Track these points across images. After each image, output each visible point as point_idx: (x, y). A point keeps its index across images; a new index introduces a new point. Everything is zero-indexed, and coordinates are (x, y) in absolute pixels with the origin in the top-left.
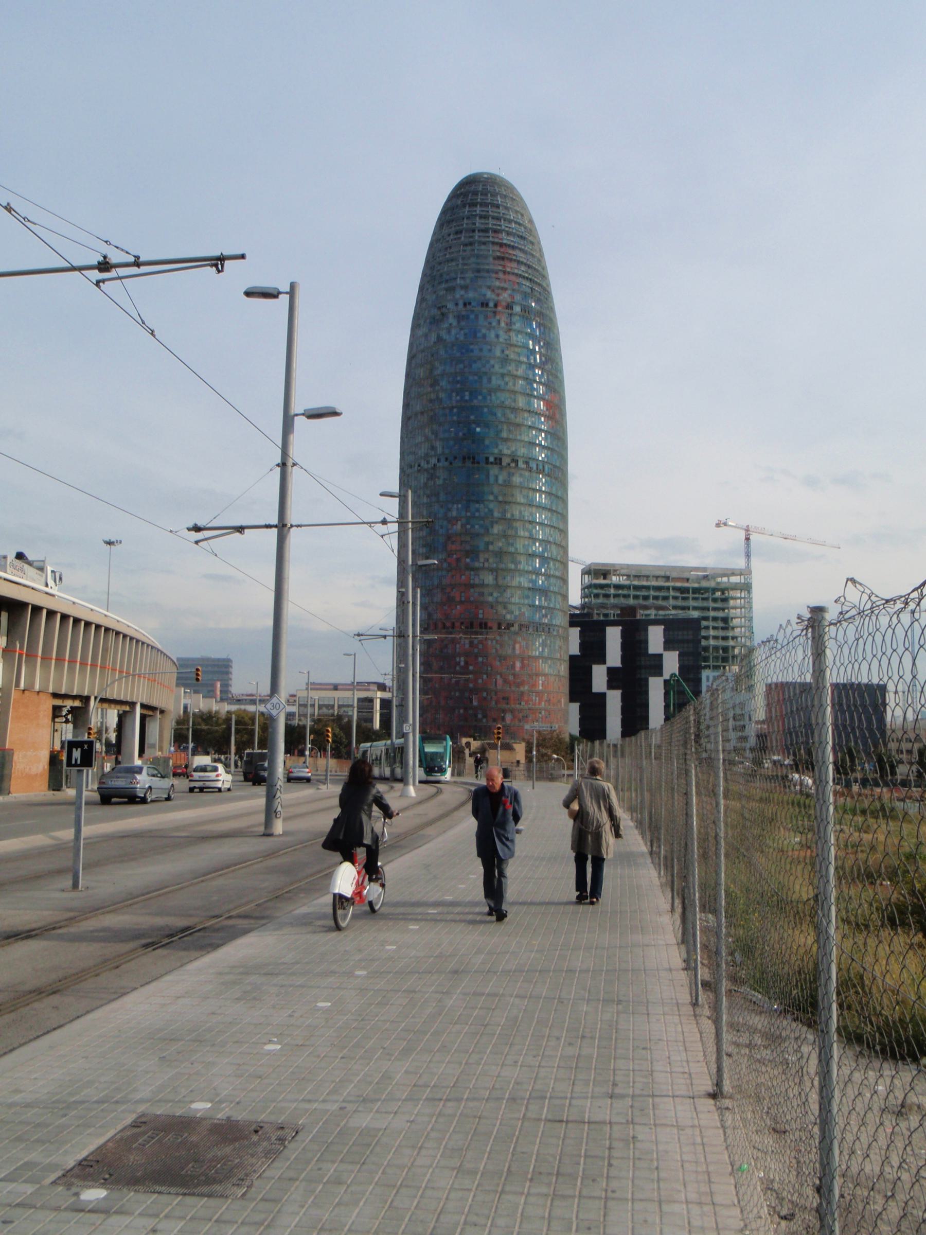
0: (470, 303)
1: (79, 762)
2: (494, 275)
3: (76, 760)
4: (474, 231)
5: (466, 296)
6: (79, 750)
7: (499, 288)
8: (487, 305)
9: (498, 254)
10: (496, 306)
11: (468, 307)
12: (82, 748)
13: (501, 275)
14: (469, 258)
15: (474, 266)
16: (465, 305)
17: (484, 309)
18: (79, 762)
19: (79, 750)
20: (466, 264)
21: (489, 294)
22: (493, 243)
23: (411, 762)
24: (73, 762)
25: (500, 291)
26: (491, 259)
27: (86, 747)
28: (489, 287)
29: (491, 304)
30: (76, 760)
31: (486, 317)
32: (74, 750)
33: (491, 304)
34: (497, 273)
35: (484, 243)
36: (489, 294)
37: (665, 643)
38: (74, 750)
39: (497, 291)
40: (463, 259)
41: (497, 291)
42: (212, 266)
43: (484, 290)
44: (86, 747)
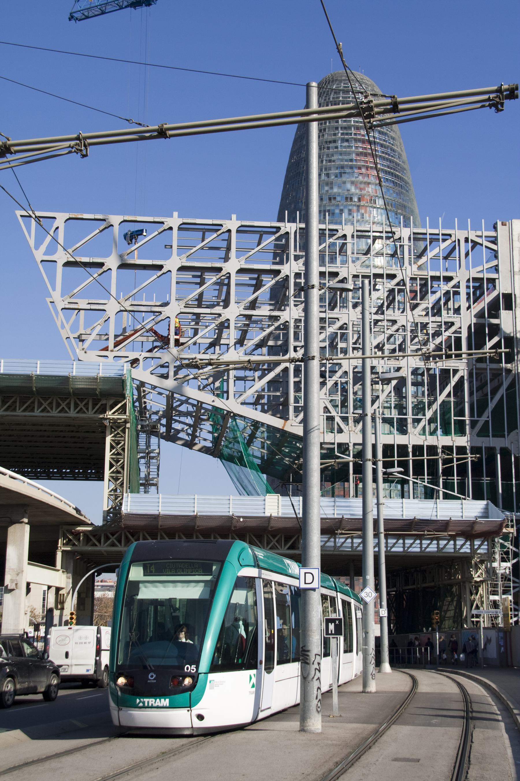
0: (335, 198)
1: (333, 632)
2: (356, 171)
3: (332, 631)
4: (337, 128)
5: (330, 191)
6: (333, 624)
7: (361, 183)
8: (351, 199)
9: (361, 150)
10: (359, 200)
11: (333, 202)
12: (335, 623)
13: (363, 171)
14: (332, 155)
15: (338, 163)
16: (330, 199)
17: (349, 203)
18: (333, 632)
19: (333, 624)
20: (330, 161)
21: (353, 190)
22: (356, 140)
23: (25, 361)
24: (330, 632)
25: (362, 186)
26: (354, 155)
27: (337, 622)
28: (352, 183)
29: (356, 199)
30: (332, 631)
31: (350, 212)
32: (330, 624)
33: (356, 199)
34: (360, 168)
35: (347, 141)
36: (353, 190)
37: (417, 446)
38: (330, 624)
39: (359, 185)
40: (328, 155)
41: (359, 185)
42: (490, 106)
43: (348, 186)
44: (337, 622)
